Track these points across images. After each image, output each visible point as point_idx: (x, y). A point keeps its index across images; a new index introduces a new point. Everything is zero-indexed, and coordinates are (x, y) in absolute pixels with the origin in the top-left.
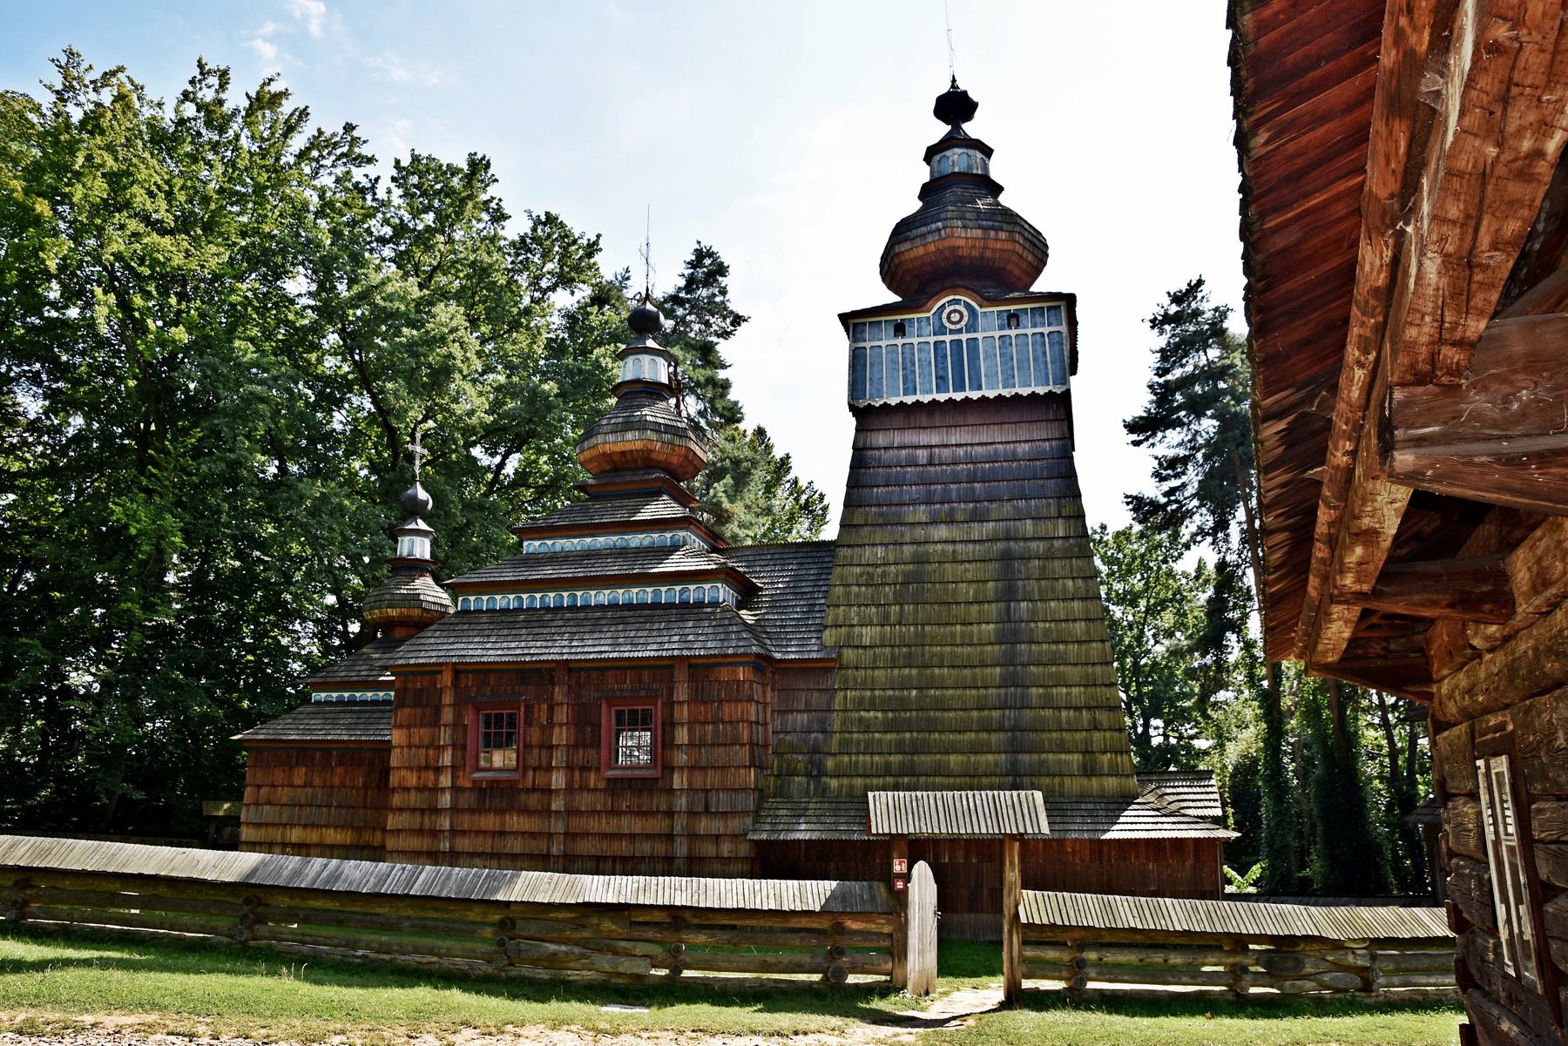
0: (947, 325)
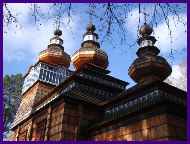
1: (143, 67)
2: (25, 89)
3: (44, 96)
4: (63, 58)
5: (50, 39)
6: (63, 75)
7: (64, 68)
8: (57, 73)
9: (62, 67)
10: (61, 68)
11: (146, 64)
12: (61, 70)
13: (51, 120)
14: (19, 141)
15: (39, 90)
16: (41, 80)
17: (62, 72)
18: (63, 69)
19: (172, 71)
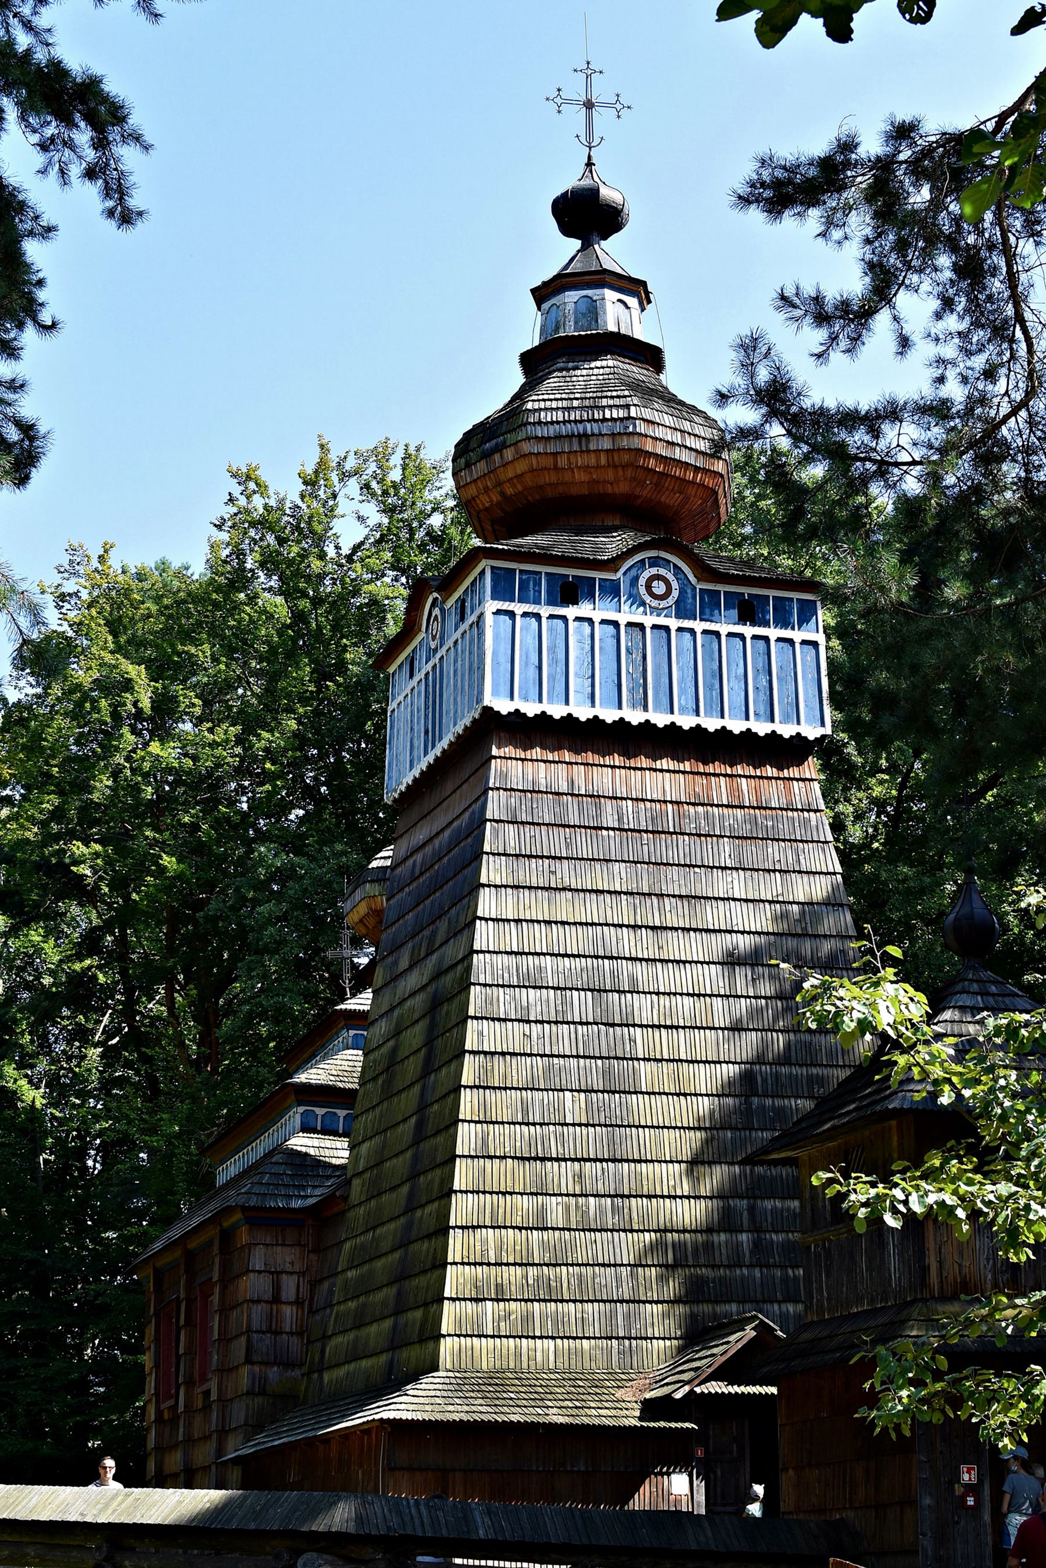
10: (654, 571)
12: (659, 588)
17: (663, 604)
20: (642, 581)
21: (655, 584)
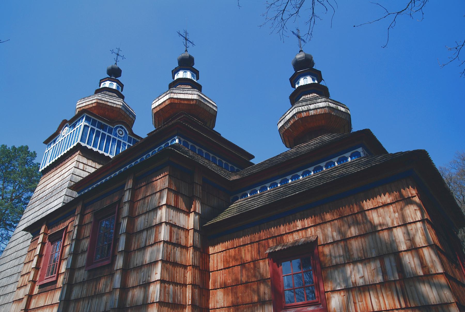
0: (118, 133)
1: (312, 114)
2: (48, 160)
3: (88, 174)
4: (123, 113)
5: (101, 80)
6: (122, 141)
7: (125, 130)
8: (112, 136)
9: (123, 128)
11: (319, 110)
12: (121, 133)
13: (132, 202)
14: (325, 291)
15: (79, 162)
16: (83, 144)
18: (123, 131)
19: (369, 130)
20: (118, 130)
21: (120, 131)
